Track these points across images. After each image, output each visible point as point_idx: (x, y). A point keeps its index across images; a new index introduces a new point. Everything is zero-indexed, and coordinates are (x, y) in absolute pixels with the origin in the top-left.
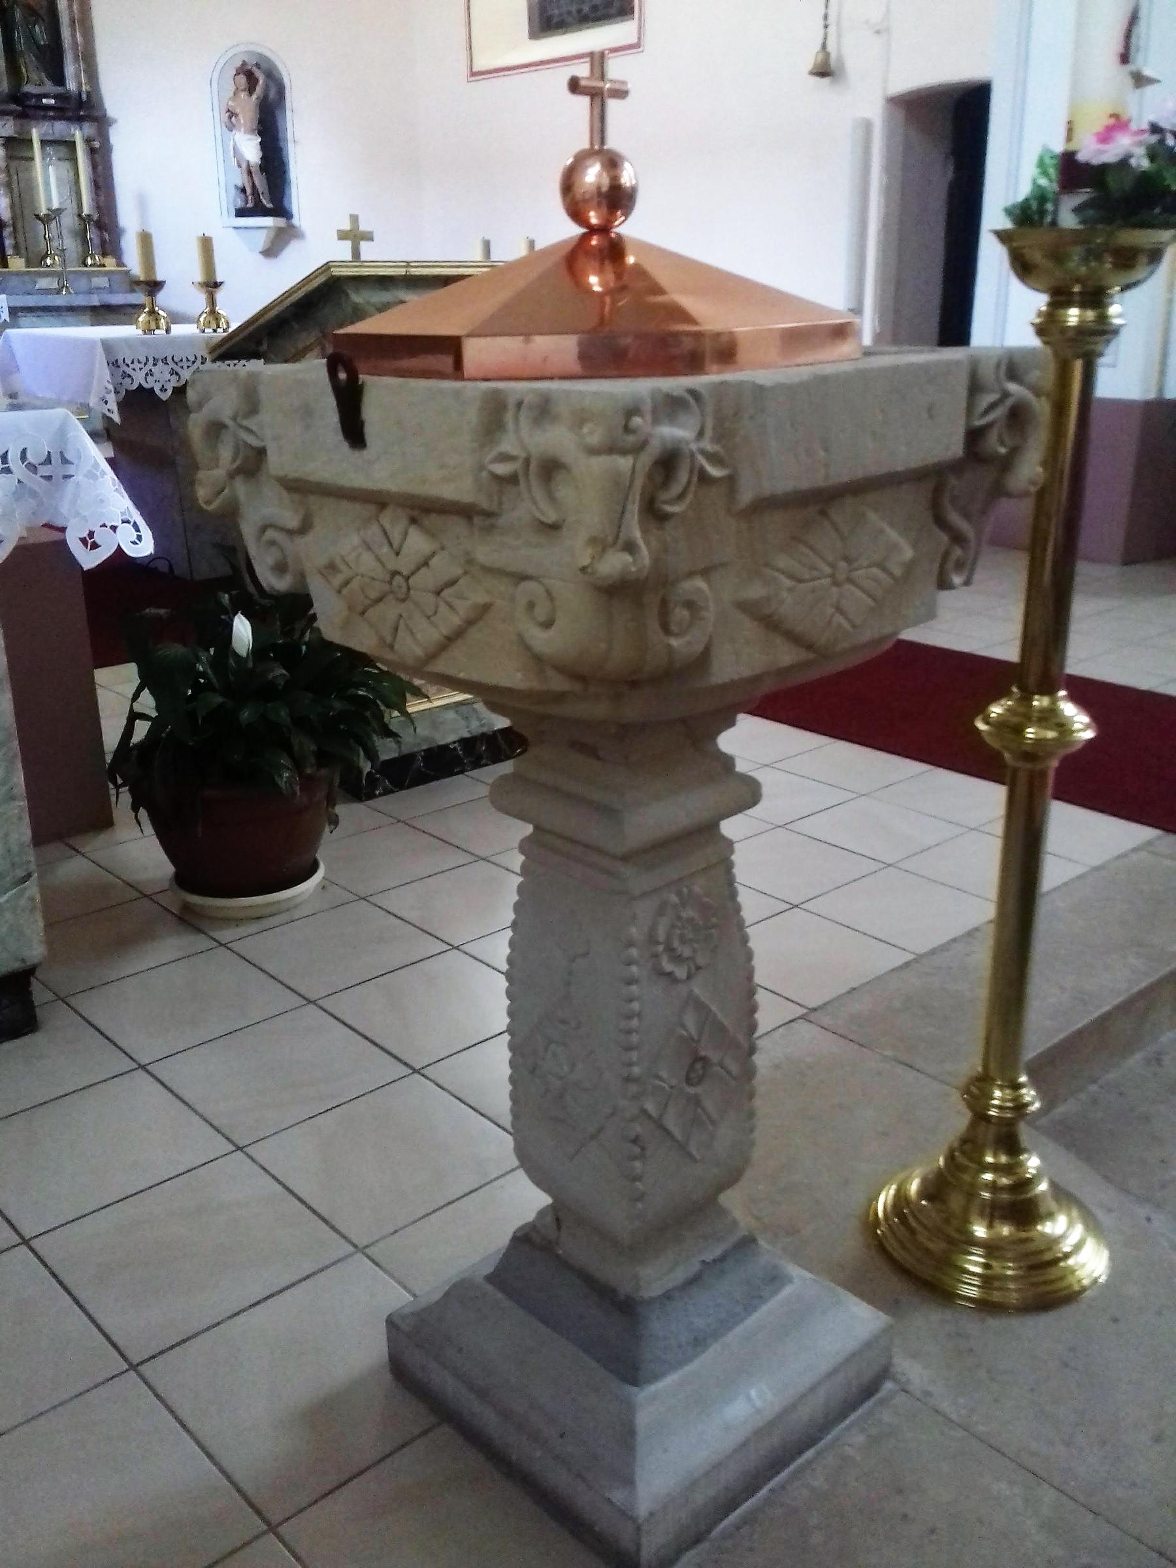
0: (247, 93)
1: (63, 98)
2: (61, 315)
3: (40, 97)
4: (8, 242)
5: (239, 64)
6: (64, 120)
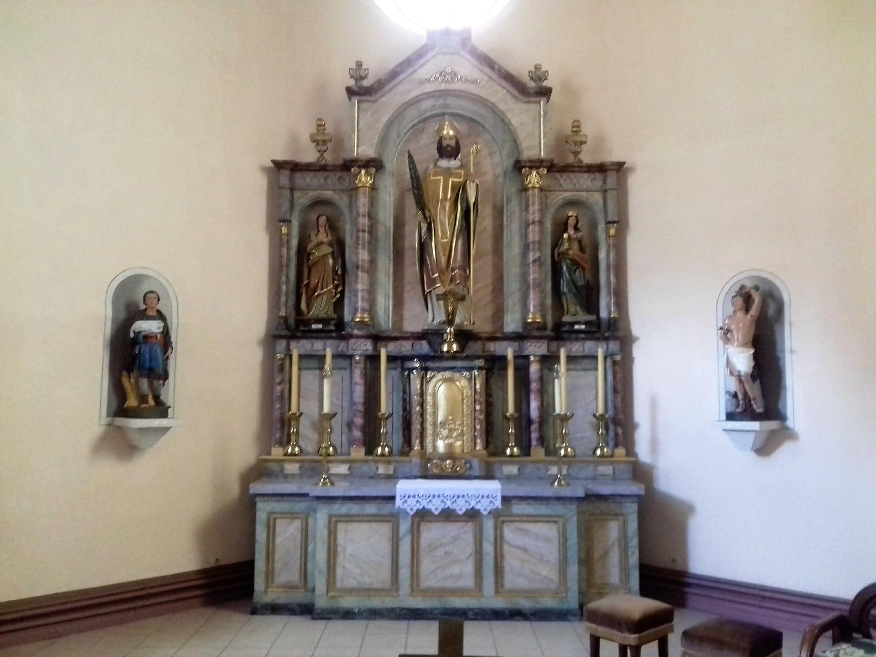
0: (743, 311)
3: (573, 324)
4: (534, 435)
5: (737, 288)
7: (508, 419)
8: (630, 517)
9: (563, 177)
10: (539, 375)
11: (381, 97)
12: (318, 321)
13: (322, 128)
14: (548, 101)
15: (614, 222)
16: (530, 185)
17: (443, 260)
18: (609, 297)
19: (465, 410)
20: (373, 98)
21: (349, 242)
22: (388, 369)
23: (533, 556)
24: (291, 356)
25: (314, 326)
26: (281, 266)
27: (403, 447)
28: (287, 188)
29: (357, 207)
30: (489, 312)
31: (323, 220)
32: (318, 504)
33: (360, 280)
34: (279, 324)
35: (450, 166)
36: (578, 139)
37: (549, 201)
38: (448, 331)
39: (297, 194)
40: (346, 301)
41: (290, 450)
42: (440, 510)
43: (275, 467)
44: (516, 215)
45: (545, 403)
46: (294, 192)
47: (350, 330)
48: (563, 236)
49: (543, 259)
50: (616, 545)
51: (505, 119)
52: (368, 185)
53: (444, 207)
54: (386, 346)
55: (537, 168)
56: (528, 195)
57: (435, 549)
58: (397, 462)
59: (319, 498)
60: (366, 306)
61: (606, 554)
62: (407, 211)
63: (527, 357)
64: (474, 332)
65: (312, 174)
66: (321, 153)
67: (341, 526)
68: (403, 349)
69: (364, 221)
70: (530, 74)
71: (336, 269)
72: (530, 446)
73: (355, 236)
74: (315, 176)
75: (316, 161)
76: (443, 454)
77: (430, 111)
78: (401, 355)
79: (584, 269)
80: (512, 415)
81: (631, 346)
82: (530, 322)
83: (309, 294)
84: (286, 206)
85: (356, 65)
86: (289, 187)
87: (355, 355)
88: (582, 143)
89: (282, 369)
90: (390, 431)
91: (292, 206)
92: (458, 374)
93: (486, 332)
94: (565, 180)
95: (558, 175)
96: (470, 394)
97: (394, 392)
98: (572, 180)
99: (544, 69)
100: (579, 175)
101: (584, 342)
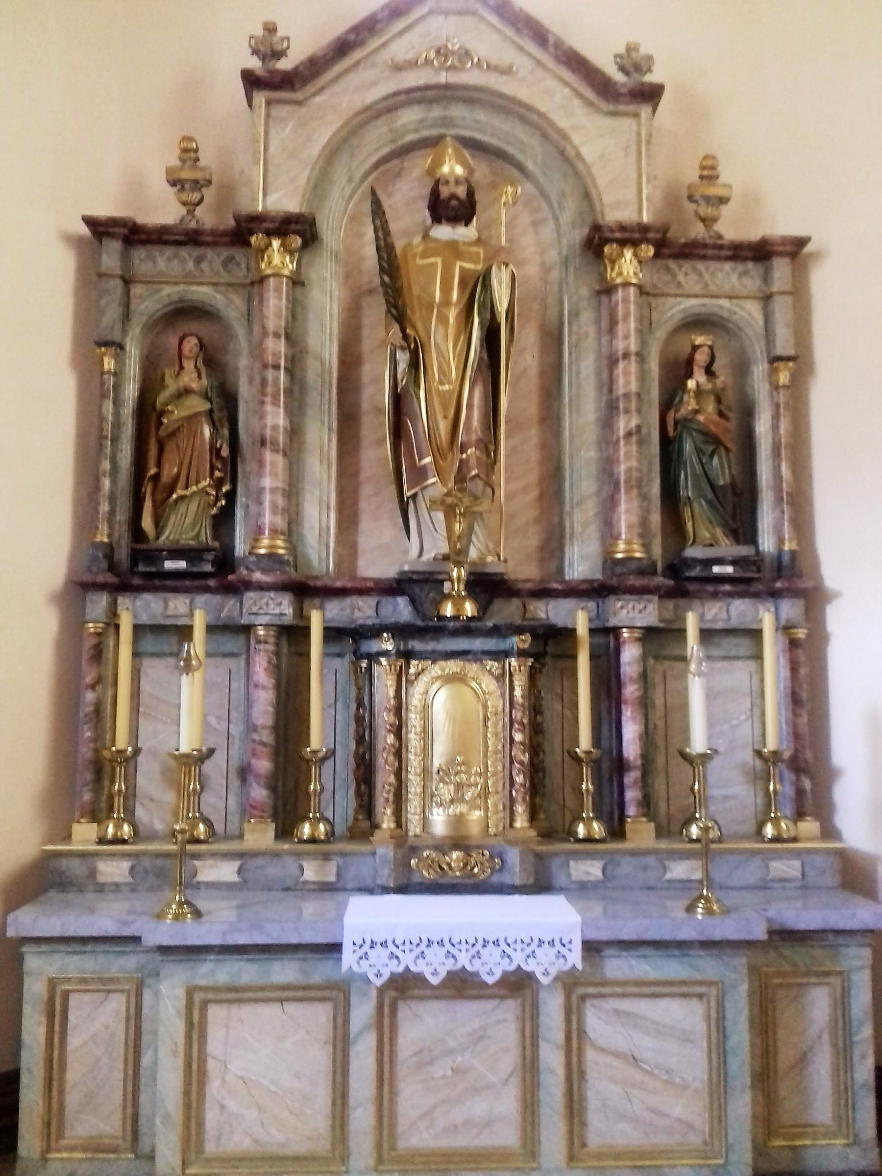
1: (754, 562)
2: (686, 955)
3: (709, 563)
4: (632, 795)
6: (749, 597)
7: (577, 760)
8: (855, 977)
9: (683, 269)
10: (641, 669)
11: (315, 94)
12: (176, 553)
13: (192, 155)
14: (654, 111)
15: (789, 359)
16: (619, 281)
17: (443, 427)
18: (778, 510)
19: (490, 743)
20: (298, 96)
21: (245, 390)
22: (325, 655)
23: (650, 1074)
24: (117, 627)
25: (169, 565)
26: (102, 438)
27: (356, 819)
28: (113, 276)
29: (263, 317)
30: (533, 540)
31: (191, 344)
32: (162, 961)
33: (268, 469)
34: (95, 559)
35: (456, 238)
36: (714, 191)
37: (655, 316)
38: (455, 574)
39: (137, 290)
40: (239, 513)
41: (111, 830)
42: (443, 974)
43: (76, 868)
44: (590, 344)
45: (651, 726)
46: (132, 286)
47: (245, 572)
48: (685, 385)
49: (644, 431)
50: (826, 1037)
51: (568, 148)
52: (286, 272)
53: (443, 320)
54: (322, 608)
55: (635, 244)
56: (613, 303)
57: (431, 1062)
58: (344, 855)
59: (164, 950)
60: (280, 522)
61: (803, 1060)
62: (365, 332)
63: (615, 631)
64: (506, 577)
65: (169, 251)
66: (188, 207)
67: (215, 1012)
68: (357, 614)
69: (277, 347)
70: (618, 60)
71: (218, 446)
72: (622, 817)
73: (257, 379)
74: (176, 256)
75: (178, 222)
76: (445, 838)
77: (416, 131)
78: (353, 626)
79: (727, 450)
80: (588, 753)
81: (823, 610)
82: (619, 559)
83: (159, 497)
84: (113, 312)
85: (265, 29)
86: (120, 273)
87: (255, 626)
88: (723, 201)
89: (98, 654)
90: (329, 786)
91: (126, 317)
92: (475, 667)
93: (527, 581)
94: (686, 274)
95: (672, 264)
96: (500, 708)
97: (339, 705)
98: (700, 275)
99: (643, 51)
100: (714, 265)
101: (729, 600)
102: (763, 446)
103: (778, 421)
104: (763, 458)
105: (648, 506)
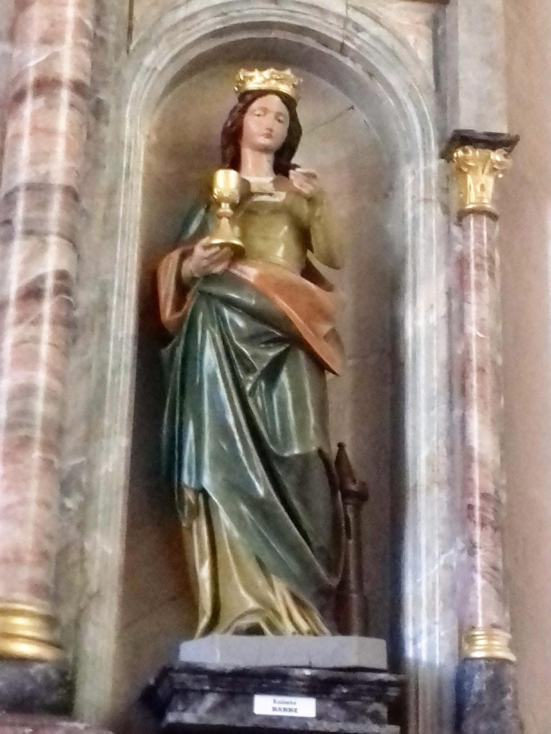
102: (422, 371)
103: (463, 300)
104: (422, 402)
105: (83, 507)
